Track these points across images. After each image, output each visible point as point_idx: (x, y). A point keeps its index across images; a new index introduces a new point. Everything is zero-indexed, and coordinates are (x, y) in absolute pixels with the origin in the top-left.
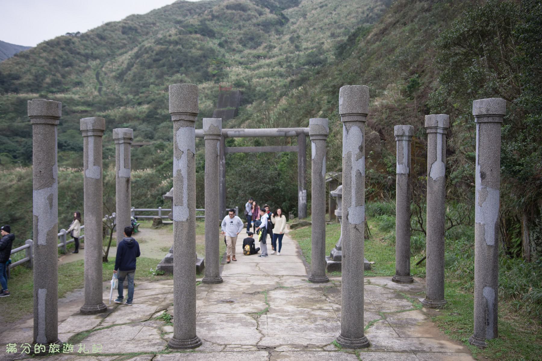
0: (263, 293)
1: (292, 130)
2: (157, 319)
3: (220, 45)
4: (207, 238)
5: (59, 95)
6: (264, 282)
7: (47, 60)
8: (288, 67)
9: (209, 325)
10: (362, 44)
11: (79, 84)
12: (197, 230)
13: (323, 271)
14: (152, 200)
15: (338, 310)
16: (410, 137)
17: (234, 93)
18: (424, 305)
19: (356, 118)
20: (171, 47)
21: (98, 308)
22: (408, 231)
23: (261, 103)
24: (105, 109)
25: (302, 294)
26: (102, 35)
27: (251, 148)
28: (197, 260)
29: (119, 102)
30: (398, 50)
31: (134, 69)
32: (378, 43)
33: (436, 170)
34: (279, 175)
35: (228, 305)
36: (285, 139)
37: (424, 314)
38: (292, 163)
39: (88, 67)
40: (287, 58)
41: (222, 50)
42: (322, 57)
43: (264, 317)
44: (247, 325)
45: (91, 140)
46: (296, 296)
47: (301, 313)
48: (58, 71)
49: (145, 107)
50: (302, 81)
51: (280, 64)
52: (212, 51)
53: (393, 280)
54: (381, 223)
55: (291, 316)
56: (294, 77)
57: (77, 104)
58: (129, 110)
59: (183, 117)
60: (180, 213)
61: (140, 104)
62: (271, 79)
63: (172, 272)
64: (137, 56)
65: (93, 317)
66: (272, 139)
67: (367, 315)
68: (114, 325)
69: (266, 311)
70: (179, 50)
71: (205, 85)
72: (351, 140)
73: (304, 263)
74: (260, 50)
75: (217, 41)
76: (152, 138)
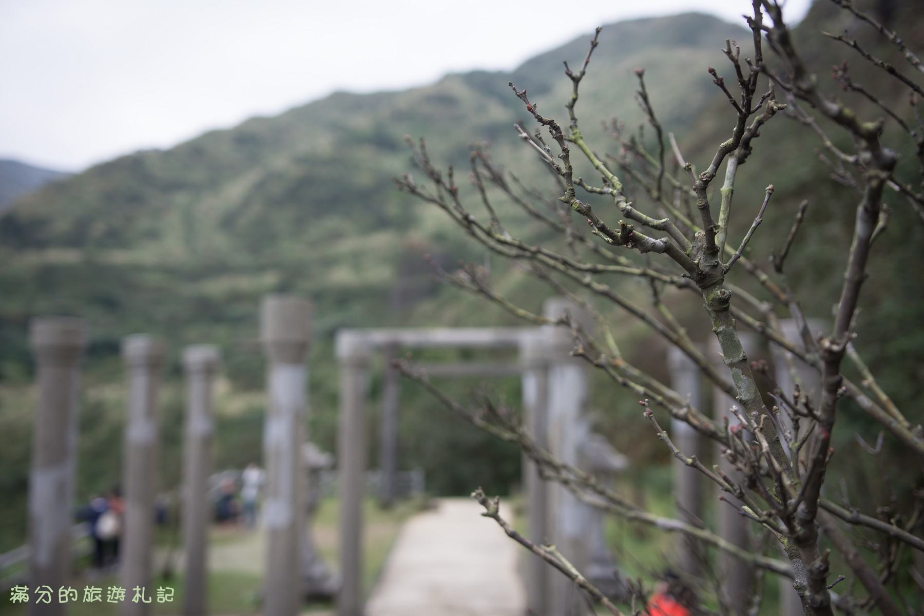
29: (219, 268)
64: (260, 186)
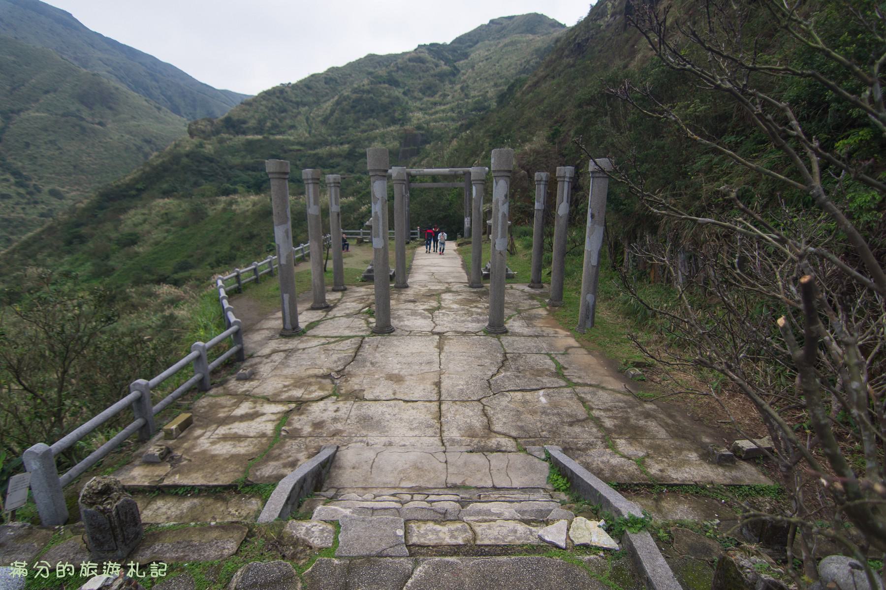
1: (460, 170)
2: (364, 313)
3: (405, 94)
4: (397, 256)
5: (278, 137)
7: (266, 107)
8: (459, 112)
9: (400, 318)
10: (518, 95)
11: (292, 127)
12: (389, 247)
13: (479, 280)
14: (354, 223)
15: (488, 308)
17: (416, 135)
18: (548, 305)
19: (503, 174)
20: (365, 96)
21: (323, 305)
22: (541, 249)
23: (437, 144)
24: (315, 148)
26: (310, 85)
27: (430, 185)
28: (389, 271)
29: (325, 143)
30: (546, 101)
31: (336, 115)
32: (531, 94)
33: (562, 209)
34: (450, 204)
35: (412, 304)
36: (455, 176)
37: (547, 310)
38: (460, 195)
39: (299, 113)
40: (458, 105)
41: (406, 98)
42: (486, 104)
43: (437, 312)
44: (425, 317)
45: (311, 186)
46: (460, 297)
47: (463, 310)
48: (276, 117)
49: (346, 147)
50: (468, 126)
51: (452, 110)
52: (398, 98)
54: (525, 243)
56: (463, 122)
57: (293, 144)
58: (334, 149)
59: (378, 173)
60: (378, 243)
61: (342, 144)
62: (445, 123)
63: (373, 280)
64: (338, 103)
66: (445, 177)
68: (335, 317)
69: (439, 308)
70: (371, 98)
71: (392, 128)
72: (500, 189)
74: (437, 98)
75: (401, 90)
76: (352, 172)
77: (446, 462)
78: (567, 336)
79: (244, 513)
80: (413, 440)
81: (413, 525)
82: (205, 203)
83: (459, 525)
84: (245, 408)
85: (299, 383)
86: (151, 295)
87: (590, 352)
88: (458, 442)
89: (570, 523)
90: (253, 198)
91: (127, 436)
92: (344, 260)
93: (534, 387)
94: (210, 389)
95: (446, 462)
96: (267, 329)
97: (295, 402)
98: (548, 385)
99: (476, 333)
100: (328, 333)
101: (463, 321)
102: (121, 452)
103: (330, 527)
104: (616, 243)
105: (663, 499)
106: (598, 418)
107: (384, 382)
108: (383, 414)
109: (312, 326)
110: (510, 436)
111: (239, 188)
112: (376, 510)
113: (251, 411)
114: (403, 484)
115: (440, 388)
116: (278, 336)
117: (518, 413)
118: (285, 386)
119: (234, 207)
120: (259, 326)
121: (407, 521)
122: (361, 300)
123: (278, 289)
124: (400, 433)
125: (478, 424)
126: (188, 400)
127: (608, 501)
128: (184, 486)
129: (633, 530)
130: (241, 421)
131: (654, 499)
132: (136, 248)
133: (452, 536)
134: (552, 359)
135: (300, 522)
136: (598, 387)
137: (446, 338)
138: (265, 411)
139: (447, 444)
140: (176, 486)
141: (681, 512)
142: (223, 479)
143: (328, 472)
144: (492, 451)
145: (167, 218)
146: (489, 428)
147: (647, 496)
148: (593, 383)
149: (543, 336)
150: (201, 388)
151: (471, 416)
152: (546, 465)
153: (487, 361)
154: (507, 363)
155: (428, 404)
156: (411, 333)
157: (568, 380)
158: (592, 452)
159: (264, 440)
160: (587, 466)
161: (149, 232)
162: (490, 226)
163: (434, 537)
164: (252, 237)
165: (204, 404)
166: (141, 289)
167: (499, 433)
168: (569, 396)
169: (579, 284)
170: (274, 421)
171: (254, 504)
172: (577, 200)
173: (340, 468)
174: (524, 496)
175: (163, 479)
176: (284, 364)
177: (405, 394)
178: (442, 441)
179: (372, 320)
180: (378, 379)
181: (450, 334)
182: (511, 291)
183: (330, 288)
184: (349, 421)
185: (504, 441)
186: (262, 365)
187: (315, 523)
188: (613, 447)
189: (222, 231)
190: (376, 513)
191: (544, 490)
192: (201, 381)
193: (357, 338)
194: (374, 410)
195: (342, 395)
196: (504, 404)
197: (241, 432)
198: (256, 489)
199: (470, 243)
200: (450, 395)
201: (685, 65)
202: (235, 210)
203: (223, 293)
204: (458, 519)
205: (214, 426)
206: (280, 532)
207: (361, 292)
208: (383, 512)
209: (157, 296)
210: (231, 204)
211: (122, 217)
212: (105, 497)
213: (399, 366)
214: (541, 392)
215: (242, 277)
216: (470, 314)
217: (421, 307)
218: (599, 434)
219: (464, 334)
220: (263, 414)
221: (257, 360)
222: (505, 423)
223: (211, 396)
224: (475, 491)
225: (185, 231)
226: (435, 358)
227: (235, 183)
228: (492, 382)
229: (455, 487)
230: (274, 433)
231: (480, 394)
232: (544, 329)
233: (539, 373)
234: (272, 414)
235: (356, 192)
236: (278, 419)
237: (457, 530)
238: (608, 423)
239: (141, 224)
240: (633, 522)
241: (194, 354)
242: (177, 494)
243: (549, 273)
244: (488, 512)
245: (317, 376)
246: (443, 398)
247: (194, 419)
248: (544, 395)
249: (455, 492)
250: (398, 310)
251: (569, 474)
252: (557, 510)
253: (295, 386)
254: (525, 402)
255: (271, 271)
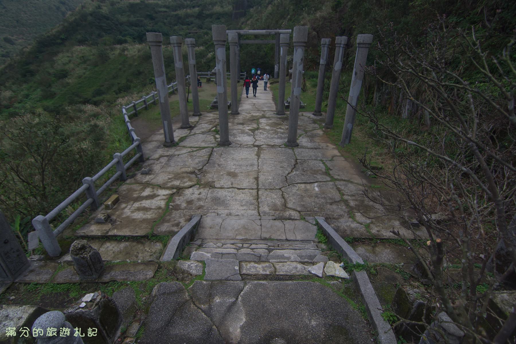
0: (256, 120)
1: (273, 31)
6: (257, 114)
13: (284, 109)
15: (287, 129)
16: (328, 45)
18: (324, 127)
22: (322, 90)
25: (273, 121)
33: (337, 66)
34: (266, 54)
35: (242, 126)
36: (269, 35)
37: (323, 131)
38: (272, 49)
44: (249, 135)
46: (270, 121)
47: (272, 130)
53: (313, 114)
55: (268, 131)
59: (220, 43)
65: (186, 130)
67: (299, 132)
69: (258, 129)
73: (276, 104)
77: (261, 225)
78: (334, 149)
79: (153, 251)
80: (243, 212)
81: (244, 264)
82: (107, 50)
83: (267, 264)
84: (147, 192)
85: (177, 176)
86: (81, 111)
87: (346, 159)
88: (267, 214)
89: (325, 264)
90: (138, 46)
91: (85, 208)
92: (199, 94)
93: (312, 181)
94: (127, 179)
95: (261, 225)
96: (156, 141)
97: (176, 188)
98: (320, 180)
99: (279, 146)
100: (192, 145)
101: (272, 138)
102: (83, 216)
103: (200, 264)
104: (369, 86)
105: (377, 246)
106: (347, 201)
107: (226, 177)
108: (226, 196)
109: (182, 139)
110: (296, 211)
111: (128, 39)
112: (224, 254)
113: (151, 193)
114: (238, 237)
115: (258, 181)
116: (162, 146)
117: (302, 197)
118: (169, 179)
119: (126, 53)
120: (150, 139)
121: (240, 262)
122: (210, 122)
123: (159, 114)
124: (236, 208)
125: (279, 203)
126: (115, 186)
127: (346, 254)
128: (120, 236)
129: (357, 270)
130: (146, 200)
131: (372, 246)
132: (67, 80)
133: (264, 270)
134: (324, 163)
135: (185, 261)
136: (349, 181)
137: (262, 149)
138: (159, 194)
139: (262, 215)
140: (115, 236)
141: (385, 256)
142: (140, 233)
143: (197, 230)
144: (286, 219)
145: (84, 60)
146: (285, 205)
147: (368, 245)
148: (346, 179)
149: (320, 148)
150: (121, 179)
151: (275, 198)
152: (315, 227)
153: (285, 165)
154: (297, 166)
155: (251, 191)
156: (241, 146)
157: (332, 177)
158: (342, 220)
159: (160, 211)
160: (337, 230)
161: (73, 69)
162: (291, 75)
163: (254, 270)
164: (140, 73)
165: (125, 189)
166: (74, 107)
167: (291, 209)
168: (331, 187)
169: (344, 113)
170: (165, 200)
171: (159, 246)
172: (348, 54)
173: (203, 228)
174: (302, 246)
175: (108, 232)
176: (167, 164)
177: (238, 184)
178: (259, 213)
179: (218, 136)
180: (222, 175)
181: (264, 146)
182: (302, 117)
183: (191, 113)
184: (207, 201)
185: (293, 213)
186: (155, 165)
187: (192, 262)
188: (353, 217)
189: (120, 69)
190: (224, 256)
191: (314, 242)
192: (121, 175)
193: (209, 149)
194: (221, 193)
195: (202, 184)
196: (294, 191)
197: (147, 206)
198: (158, 238)
199: (278, 82)
200: (263, 185)
201: (408, 69)
202: (127, 55)
203: (126, 118)
204: (267, 261)
205: (132, 202)
206: (175, 266)
207: (210, 117)
208: (227, 255)
209: (85, 112)
210: (124, 50)
211: (55, 58)
212: (83, 251)
213: (234, 167)
214: (316, 184)
215: (137, 106)
216: (276, 133)
217: (247, 128)
218: (347, 210)
219: (273, 146)
220: (158, 196)
221: (152, 162)
222: (294, 203)
223: (128, 184)
224: (276, 242)
225: (96, 69)
226: (255, 162)
227: (124, 36)
228: (288, 178)
229: (265, 239)
230: (166, 207)
231: (281, 185)
232: (320, 143)
233: (315, 172)
234: (164, 195)
235: (205, 43)
236: (167, 199)
237: (266, 267)
238: (352, 203)
239: (68, 64)
240: (358, 266)
241: (115, 160)
242: (116, 240)
243: (326, 105)
244: (283, 257)
245: (187, 173)
246: (259, 187)
247: (120, 198)
248: (317, 186)
249: (265, 242)
250: (233, 130)
251: (327, 235)
252: (319, 256)
253: (175, 179)
254: (306, 190)
255: (154, 102)
